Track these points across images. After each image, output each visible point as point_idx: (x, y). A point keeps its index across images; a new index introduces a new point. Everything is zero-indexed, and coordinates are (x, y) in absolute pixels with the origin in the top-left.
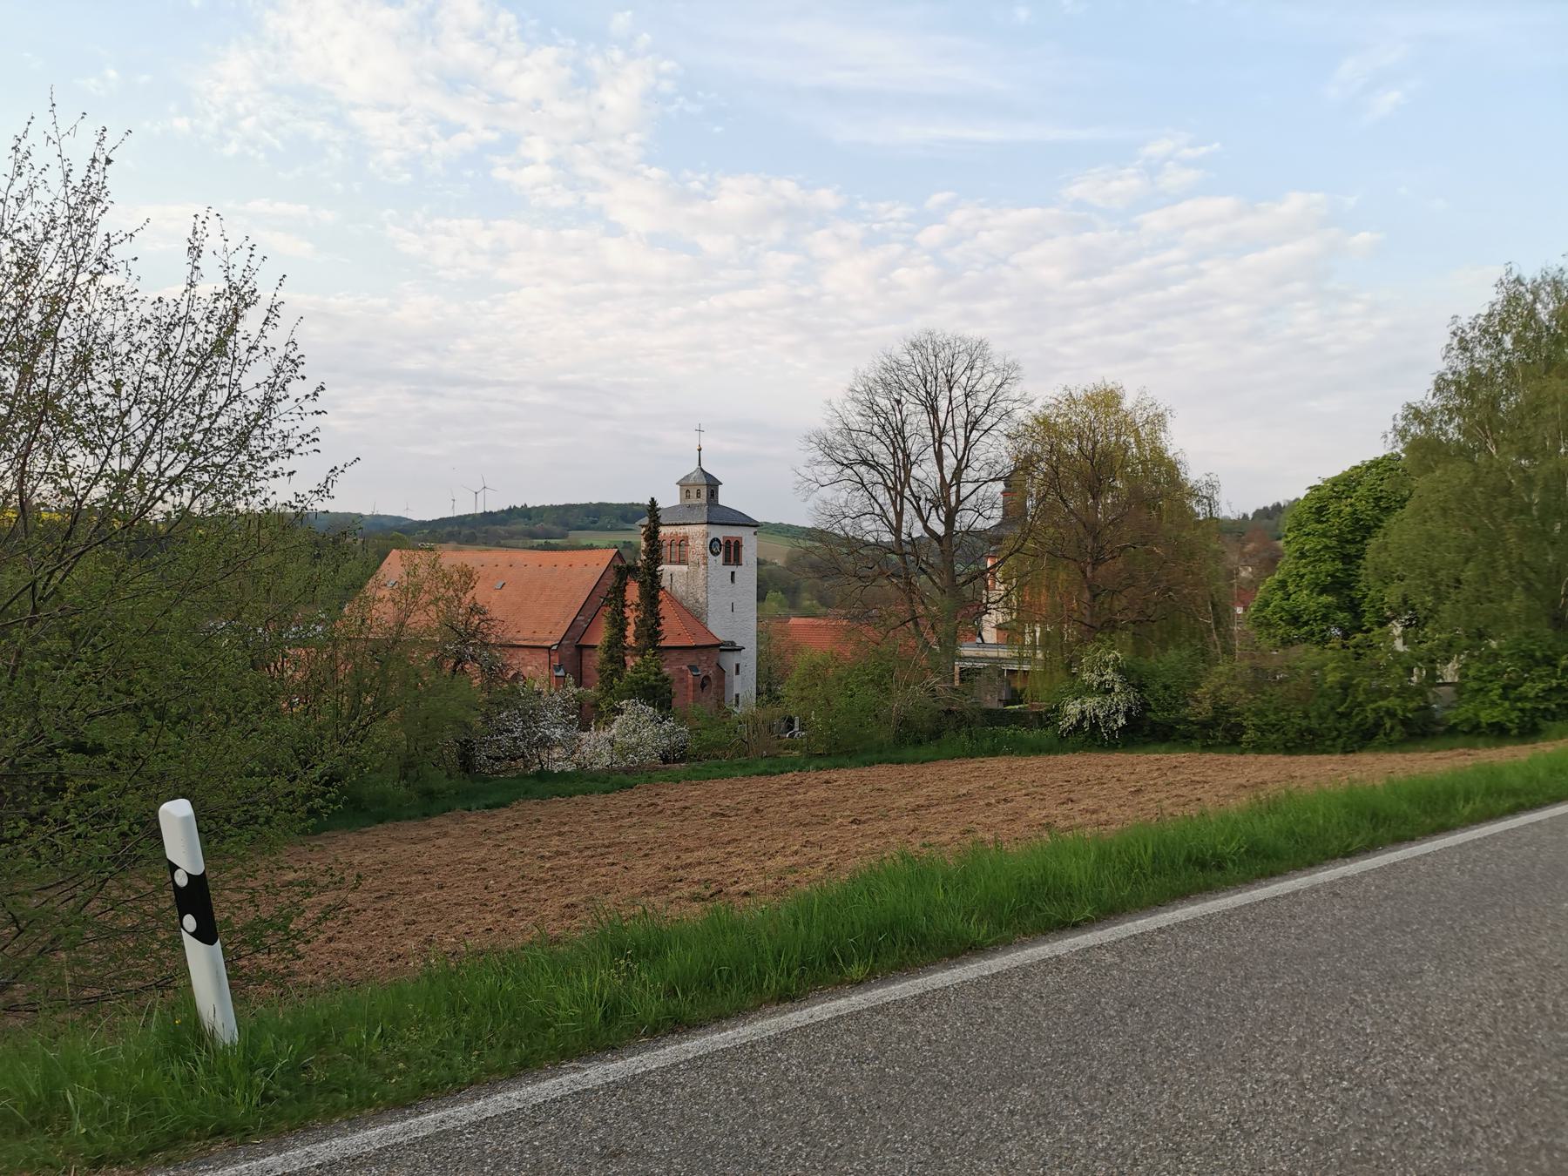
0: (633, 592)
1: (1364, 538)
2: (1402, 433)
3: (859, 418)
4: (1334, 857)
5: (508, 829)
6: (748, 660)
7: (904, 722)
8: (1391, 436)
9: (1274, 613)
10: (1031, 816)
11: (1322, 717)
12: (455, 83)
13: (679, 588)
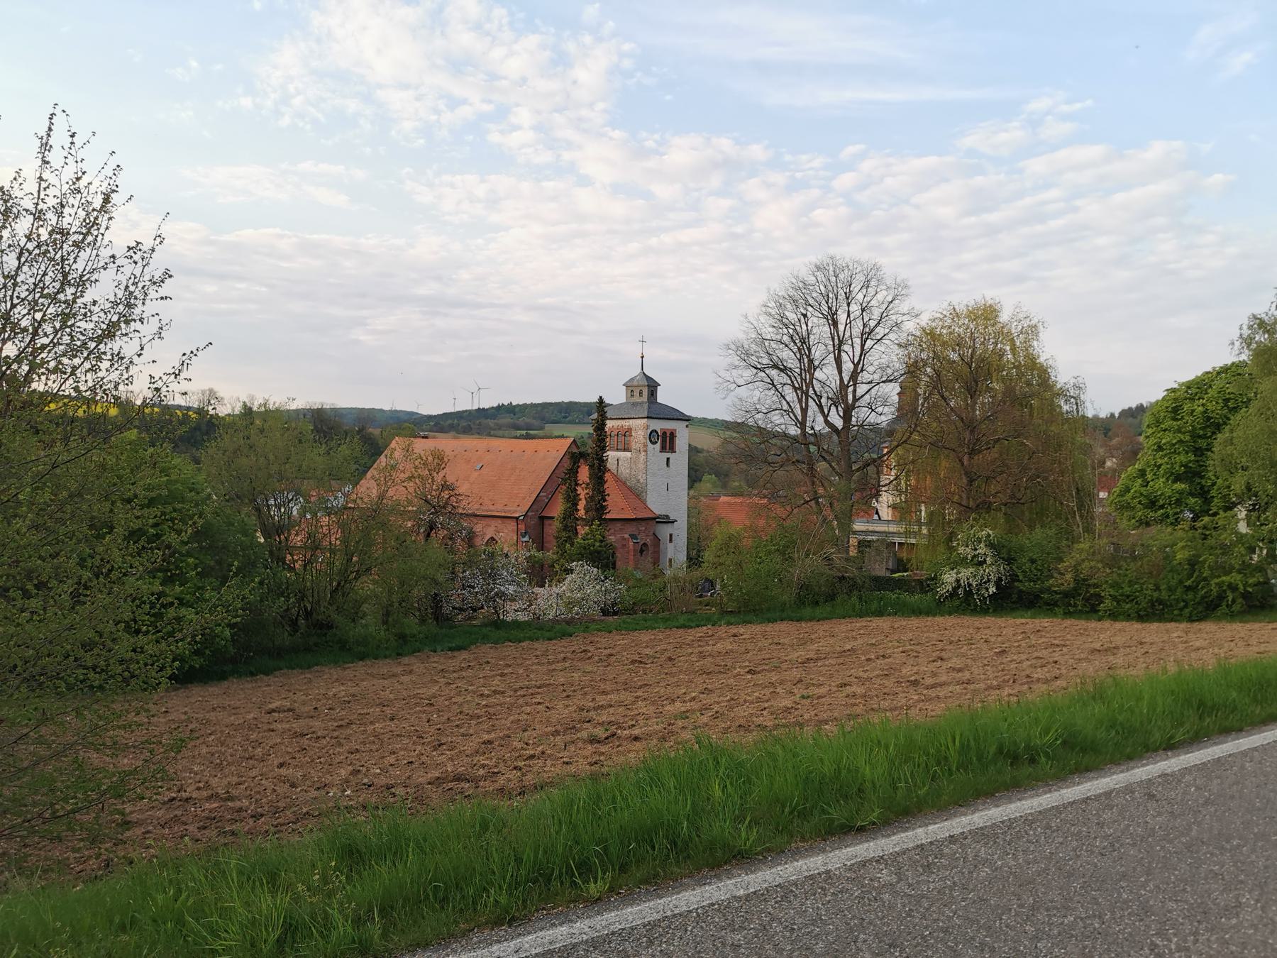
0: (584, 474)
1: (1214, 433)
2: (1248, 341)
3: (771, 329)
4: (1156, 750)
5: (462, 669)
6: (680, 530)
7: (804, 587)
8: (1237, 344)
9: (1134, 498)
10: (904, 671)
11: (1171, 590)
12: (459, 66)
13: (624, 471)
